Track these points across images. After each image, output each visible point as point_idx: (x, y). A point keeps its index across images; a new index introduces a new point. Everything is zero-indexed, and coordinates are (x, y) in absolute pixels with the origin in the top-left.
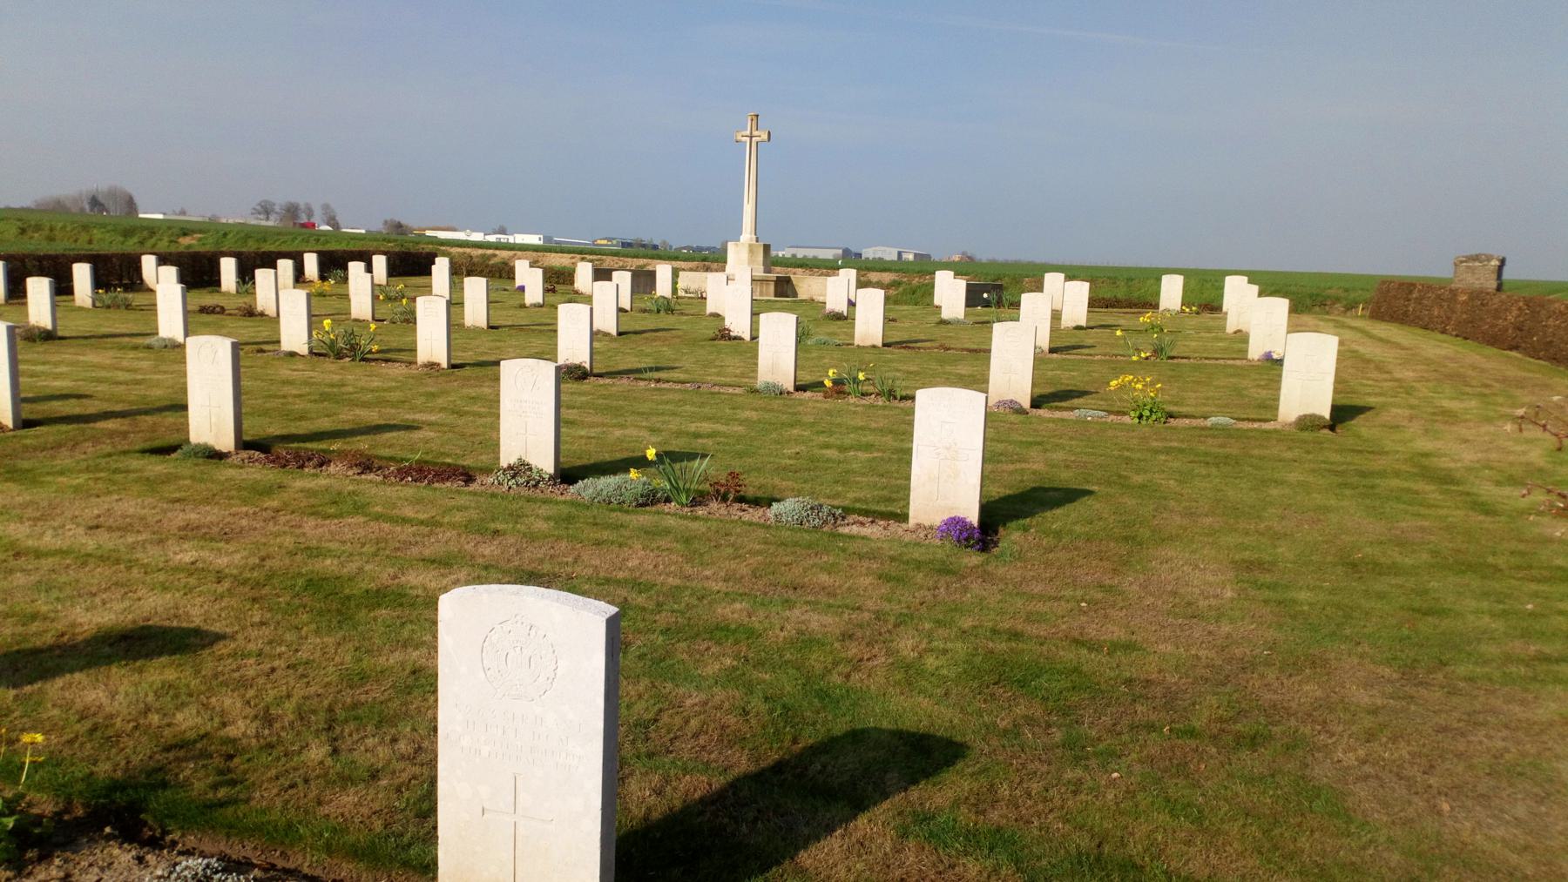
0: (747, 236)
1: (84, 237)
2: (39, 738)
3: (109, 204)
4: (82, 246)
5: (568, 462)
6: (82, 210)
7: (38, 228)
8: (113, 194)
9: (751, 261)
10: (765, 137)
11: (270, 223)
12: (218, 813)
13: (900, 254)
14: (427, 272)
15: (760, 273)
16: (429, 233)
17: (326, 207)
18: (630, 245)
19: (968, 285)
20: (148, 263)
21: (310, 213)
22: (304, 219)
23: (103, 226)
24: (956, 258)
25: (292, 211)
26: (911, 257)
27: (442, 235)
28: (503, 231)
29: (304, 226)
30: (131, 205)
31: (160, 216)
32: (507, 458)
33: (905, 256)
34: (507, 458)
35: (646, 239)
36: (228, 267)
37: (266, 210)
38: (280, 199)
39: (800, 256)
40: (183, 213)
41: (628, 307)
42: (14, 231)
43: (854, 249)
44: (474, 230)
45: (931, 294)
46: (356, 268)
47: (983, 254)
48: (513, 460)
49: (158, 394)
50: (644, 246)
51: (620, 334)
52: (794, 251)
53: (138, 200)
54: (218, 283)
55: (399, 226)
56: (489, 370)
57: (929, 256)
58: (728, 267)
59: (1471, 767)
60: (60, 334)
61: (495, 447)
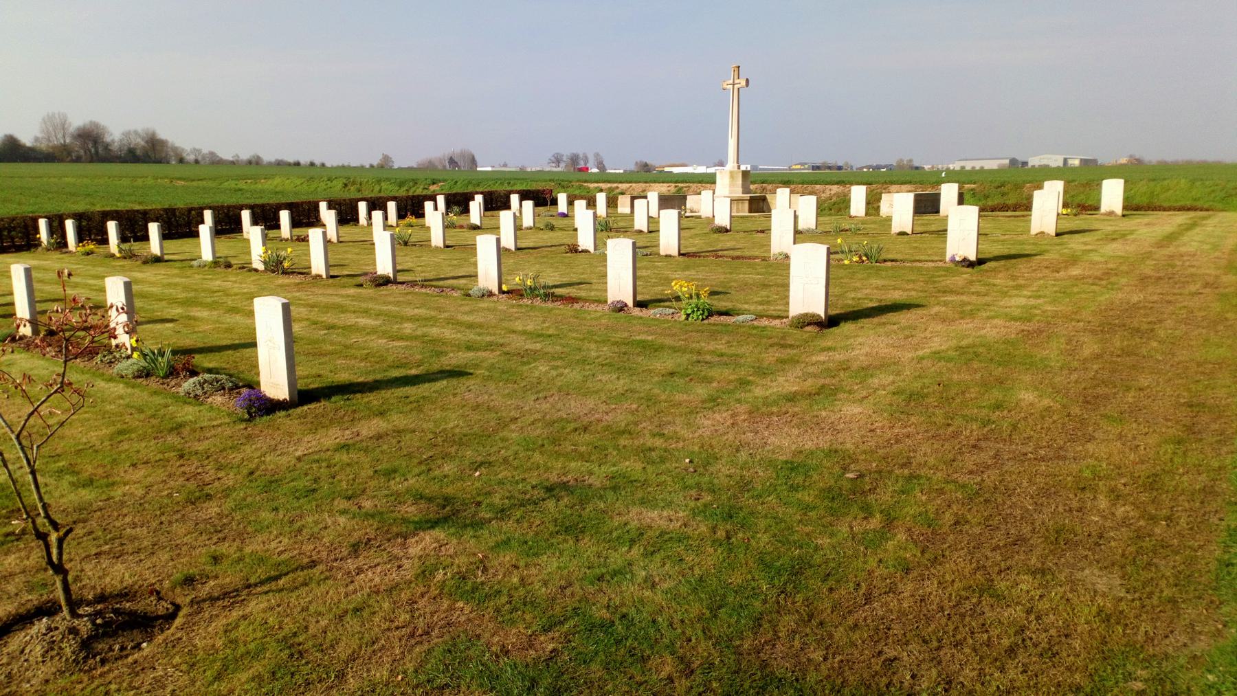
0: (731, 164)
1: (377, 188)
3: (461, 163)
4: (208, 201)
5: (833, 312)
6: (444, 167)
7: (354, 183)
8: (463, 155)
9: (732, 185)
10: (743, 83)
11: (559, 169)
12: (433, 512)
13: (1065, 160)
15: (738, 192)
16: (667, 169)
17: (597, 155)
18: (818, 168)
19: (917, 196)
20: (323, 206)
21: (586, 161)
22: (582, 165)
23: (388, 179)
24: (1124, 160)
25: (574, 159)
26: (1076, 162)
27: (676, 170)
29: (581, 170)
30: (473, 162)
31: (489, 169)
33: (1070, 162)
37: (557, 160)
38: (567, 152)
39: (968, 168)
40: (505, 165)
41: (334, 239)
42: (340, 185)
43: (1021, 158)
45: (848, 207)
46: (428, 205)
47: (1152, 154)
50: (830, 168)
51: (518, 249)
52: (962, 163)
53: (477, 158)
54: (357, 220)
55: (646, 165)
57: (1095, 161)
60: (166, 257)
61: (785, 299)
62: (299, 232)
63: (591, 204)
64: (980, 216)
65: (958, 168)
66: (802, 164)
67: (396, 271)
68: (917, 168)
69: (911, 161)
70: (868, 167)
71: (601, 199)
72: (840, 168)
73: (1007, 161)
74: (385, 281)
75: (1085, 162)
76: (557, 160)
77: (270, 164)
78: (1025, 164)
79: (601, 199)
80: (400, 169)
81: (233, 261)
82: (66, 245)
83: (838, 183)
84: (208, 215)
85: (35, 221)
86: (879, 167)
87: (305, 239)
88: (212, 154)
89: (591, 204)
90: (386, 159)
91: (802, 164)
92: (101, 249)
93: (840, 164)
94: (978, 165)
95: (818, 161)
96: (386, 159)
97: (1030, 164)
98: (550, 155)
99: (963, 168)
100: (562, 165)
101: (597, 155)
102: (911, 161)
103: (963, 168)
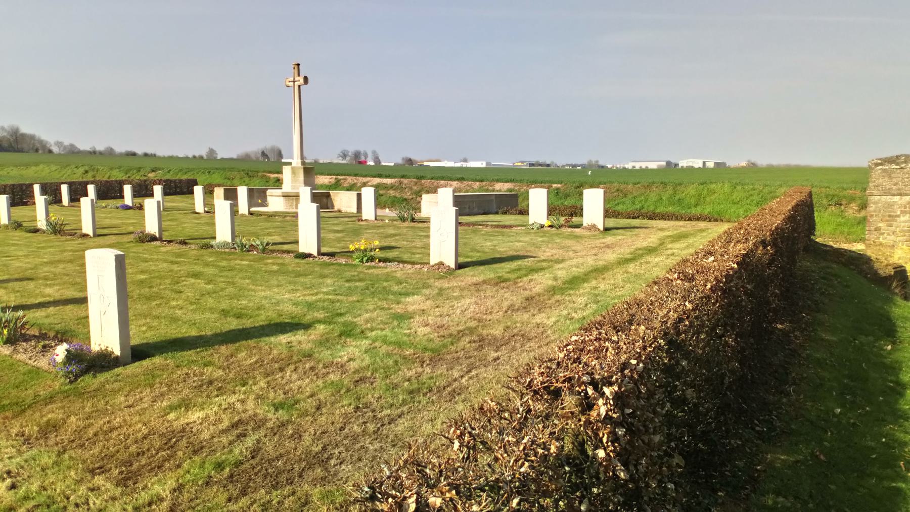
2: (779, 326)
5: (461, 260)
10: (302, 81)
11: (344, 162)
13: (704, 163)
14: (192, 192)
16: (425, 164)
17: (374, 152)
21: (366, 156)
22: (363, 159)
27: (432, 164)
28: (465, 161)
29: (360, 163)
32: (433, 261)
33: (708, 164)
34: (433, 261)
35: (541, 161)
36: (127, 190)
38: (351, 149)
39: (637, 167)
43: (674, 161)
44: (448, 160)
48: (436, 262)
49: (292, 239)
50: (541, 165)
52: (634, 164)
53: (283, 153)
55: (410, 160)
56: (425, 225)
57: (724, 164)
58: (283, 186)
59: (305, 414)
62: (138, 200)
63: (231, 195)
64: (458, 224)
65: (630, 168)
66: (522, 162)
67: (161, 230)
68: (603, 167)
69: (597, 162)
70: (569, 165)
71: (242, 192)
72: (548, 165)
73: (664, 163)
74: (153, 238)
75: (717, 164)
76: (344, 155)
77: (121, 155)
78: (676, 165)
79: (242, 192)
80: (222, 159)
81: (25, 224)
82: (60, 201)
83: (459, 180)
84: (91, 189)
85: (31, 186)
86: (575, 166)
87: (141, 208)
88: (72, 145)
89: (231, 195)
90: (212, 152)
91: (522, 162)
92: (118, 203)
93: (548, 162)
94: (644, 165)
95: (533, 160)
96: (212, 152)
97: (680, 166)
98: (339, 151)
99: (634, 167)
100: (348, 158)
101: (374, 152)
102: (597, 162)
103: (634, 167)
